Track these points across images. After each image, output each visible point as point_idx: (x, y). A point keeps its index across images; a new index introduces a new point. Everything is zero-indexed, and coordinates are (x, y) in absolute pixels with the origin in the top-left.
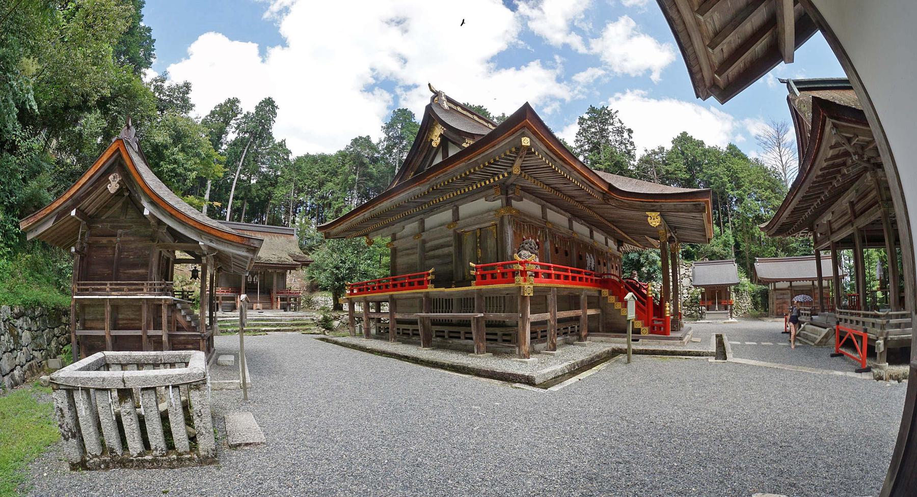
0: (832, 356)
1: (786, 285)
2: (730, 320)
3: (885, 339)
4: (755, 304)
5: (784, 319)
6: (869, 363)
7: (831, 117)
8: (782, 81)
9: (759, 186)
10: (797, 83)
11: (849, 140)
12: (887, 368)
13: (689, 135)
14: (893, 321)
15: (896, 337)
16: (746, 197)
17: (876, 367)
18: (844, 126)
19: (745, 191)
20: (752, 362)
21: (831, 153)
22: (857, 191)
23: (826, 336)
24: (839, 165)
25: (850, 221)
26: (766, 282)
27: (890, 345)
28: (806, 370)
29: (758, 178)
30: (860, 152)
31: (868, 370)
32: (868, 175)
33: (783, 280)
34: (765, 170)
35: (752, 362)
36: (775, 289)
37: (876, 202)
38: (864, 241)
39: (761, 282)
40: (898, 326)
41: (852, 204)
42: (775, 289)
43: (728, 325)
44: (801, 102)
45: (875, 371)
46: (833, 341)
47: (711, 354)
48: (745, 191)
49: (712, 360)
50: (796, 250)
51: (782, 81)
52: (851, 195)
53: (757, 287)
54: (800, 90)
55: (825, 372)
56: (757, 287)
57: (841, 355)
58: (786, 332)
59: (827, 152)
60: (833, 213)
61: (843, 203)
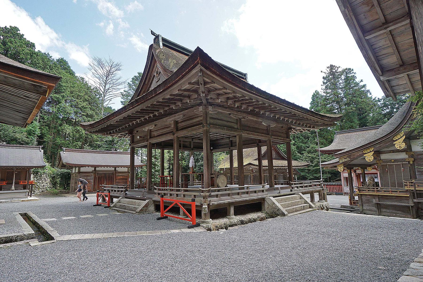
0: (159, 219)
1: (91, 169)
2: (29, 198)
3: (209, 205)
4: (54, 184)
5: (96, 195)
6: (198, 221)
7: (202, 65)
8: (153, 33)
9: (78, 97)
10: (164, 40)
11: (205, 83)
12: (212, 223)
13: (21, 32)
14: (213, 194)
15: (216, 203)
16: (63, 102)
17: (203, 222)
18: (207, 74)
19: (63, 97)
20: (87, 236)
21: (187, 86)
22: (184, 116)
23: (146, 206)
24: (185, 96)
25: (172, 132)
26: (71, 166)
27: (211, 208)
28: (145, 233)
29: (80, 91)
30: (206, 92)
31: (198, 225)
32: (201, 108)
33: (88, 166)
34: (89, 88)
35: (87, 236)
36: (79, 172)
37: (202, 124)
38: (180, 146)
39: (64, 166)
40: (217, 196)
41: (176, 123)
42: (79, 172)
43: (29, 203)
44: (161, 52)
45: (205, 225)
46: (152, 208)
47: (30, 237)
48: (63, 97)
49: (35, 243)
50: (99, 146)
51: (153, 33)
52: (179, 117)
53: (57, 170)
54: (164, 45)
55: (164, 232)
56: (57, 170)
57: (166, 217)
58: (98, 205)
59: (184, 84)
60: (155, 125)
61: (170, 121)
